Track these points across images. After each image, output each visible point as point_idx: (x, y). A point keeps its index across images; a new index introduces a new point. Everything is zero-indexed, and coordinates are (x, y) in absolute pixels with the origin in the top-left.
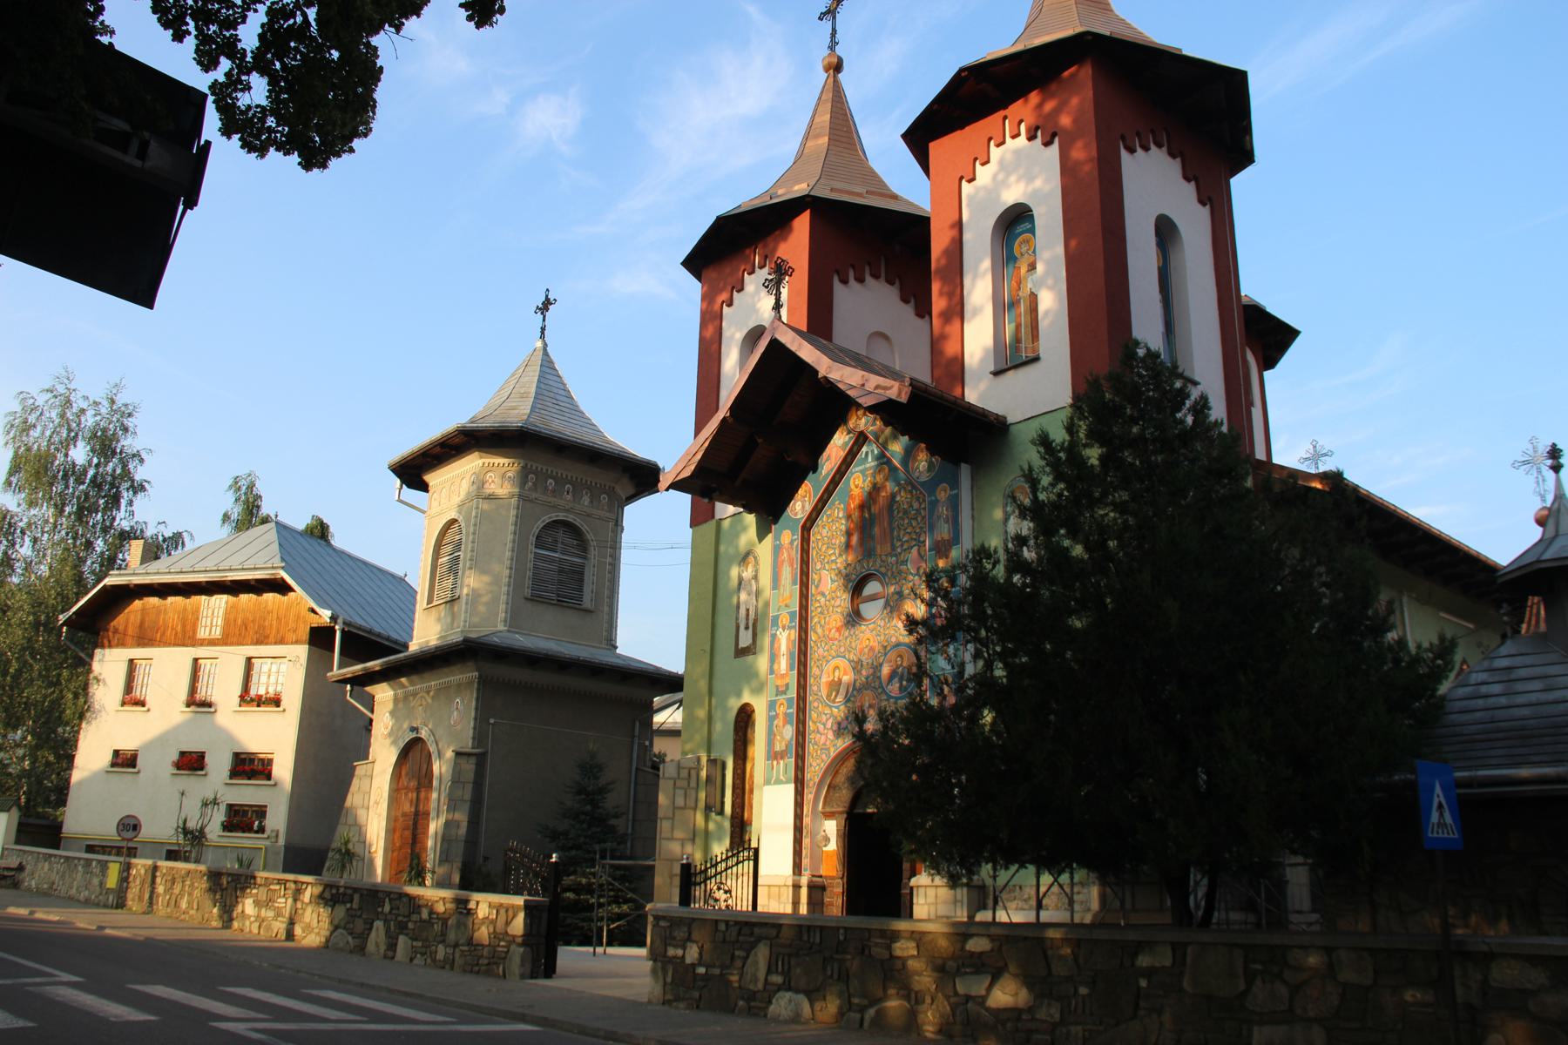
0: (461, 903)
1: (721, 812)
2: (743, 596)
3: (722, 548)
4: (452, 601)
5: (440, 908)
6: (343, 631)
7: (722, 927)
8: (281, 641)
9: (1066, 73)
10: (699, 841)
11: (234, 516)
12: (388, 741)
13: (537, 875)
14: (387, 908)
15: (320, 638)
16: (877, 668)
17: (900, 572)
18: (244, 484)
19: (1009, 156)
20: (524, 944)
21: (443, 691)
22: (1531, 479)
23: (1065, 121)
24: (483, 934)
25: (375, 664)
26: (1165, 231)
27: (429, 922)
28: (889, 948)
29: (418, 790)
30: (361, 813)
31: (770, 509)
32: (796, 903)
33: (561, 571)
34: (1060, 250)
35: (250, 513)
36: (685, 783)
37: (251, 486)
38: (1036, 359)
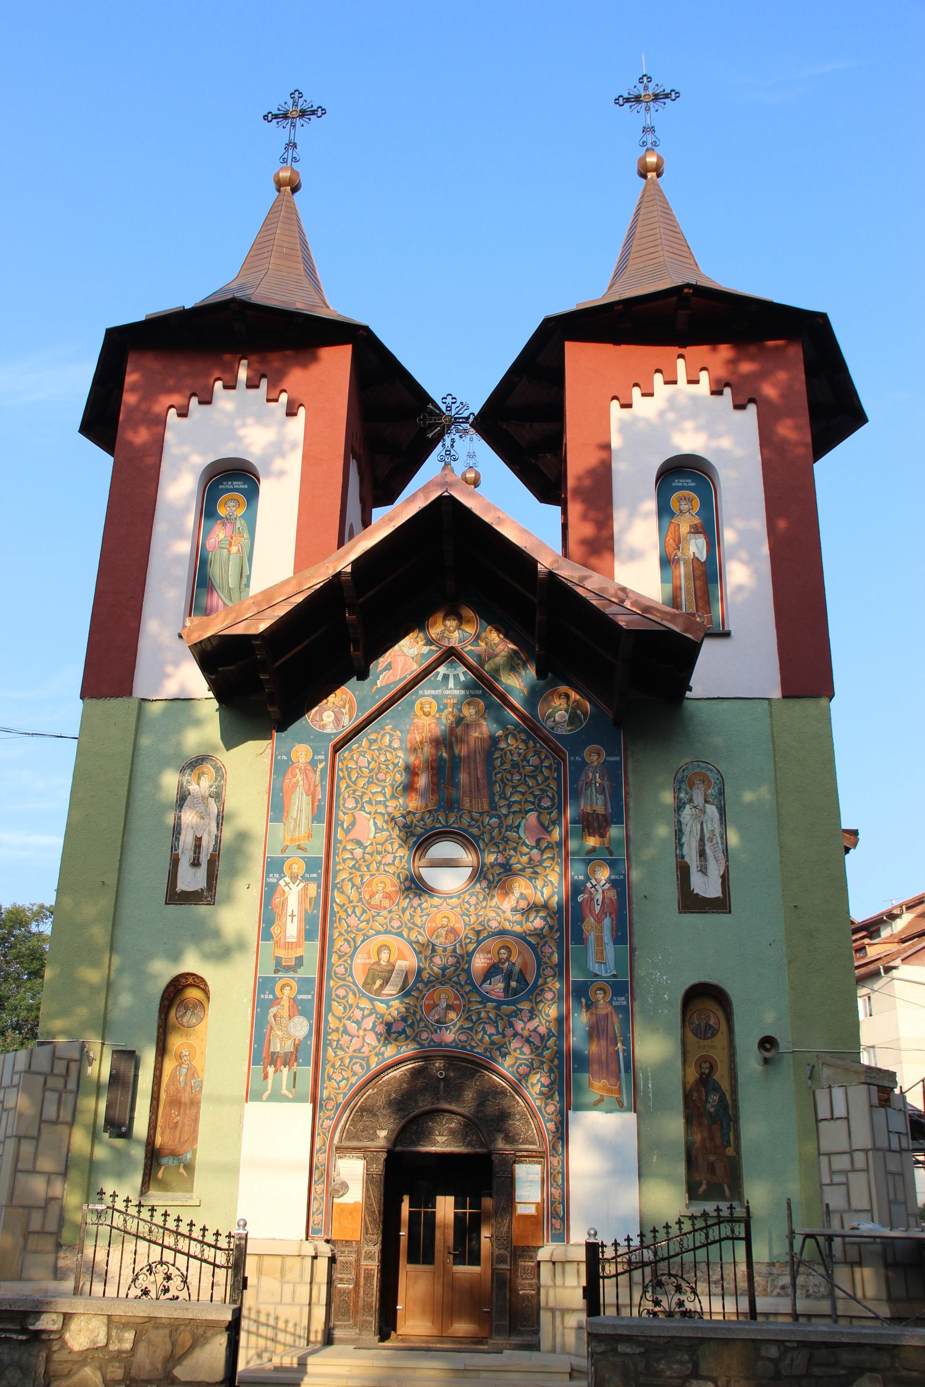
2: (189, 817)
9: (770, 343)
17: (506, 840)
23: (769, 391)
34: (759, 524)
35: (665, 103)
36: (59, 1083)
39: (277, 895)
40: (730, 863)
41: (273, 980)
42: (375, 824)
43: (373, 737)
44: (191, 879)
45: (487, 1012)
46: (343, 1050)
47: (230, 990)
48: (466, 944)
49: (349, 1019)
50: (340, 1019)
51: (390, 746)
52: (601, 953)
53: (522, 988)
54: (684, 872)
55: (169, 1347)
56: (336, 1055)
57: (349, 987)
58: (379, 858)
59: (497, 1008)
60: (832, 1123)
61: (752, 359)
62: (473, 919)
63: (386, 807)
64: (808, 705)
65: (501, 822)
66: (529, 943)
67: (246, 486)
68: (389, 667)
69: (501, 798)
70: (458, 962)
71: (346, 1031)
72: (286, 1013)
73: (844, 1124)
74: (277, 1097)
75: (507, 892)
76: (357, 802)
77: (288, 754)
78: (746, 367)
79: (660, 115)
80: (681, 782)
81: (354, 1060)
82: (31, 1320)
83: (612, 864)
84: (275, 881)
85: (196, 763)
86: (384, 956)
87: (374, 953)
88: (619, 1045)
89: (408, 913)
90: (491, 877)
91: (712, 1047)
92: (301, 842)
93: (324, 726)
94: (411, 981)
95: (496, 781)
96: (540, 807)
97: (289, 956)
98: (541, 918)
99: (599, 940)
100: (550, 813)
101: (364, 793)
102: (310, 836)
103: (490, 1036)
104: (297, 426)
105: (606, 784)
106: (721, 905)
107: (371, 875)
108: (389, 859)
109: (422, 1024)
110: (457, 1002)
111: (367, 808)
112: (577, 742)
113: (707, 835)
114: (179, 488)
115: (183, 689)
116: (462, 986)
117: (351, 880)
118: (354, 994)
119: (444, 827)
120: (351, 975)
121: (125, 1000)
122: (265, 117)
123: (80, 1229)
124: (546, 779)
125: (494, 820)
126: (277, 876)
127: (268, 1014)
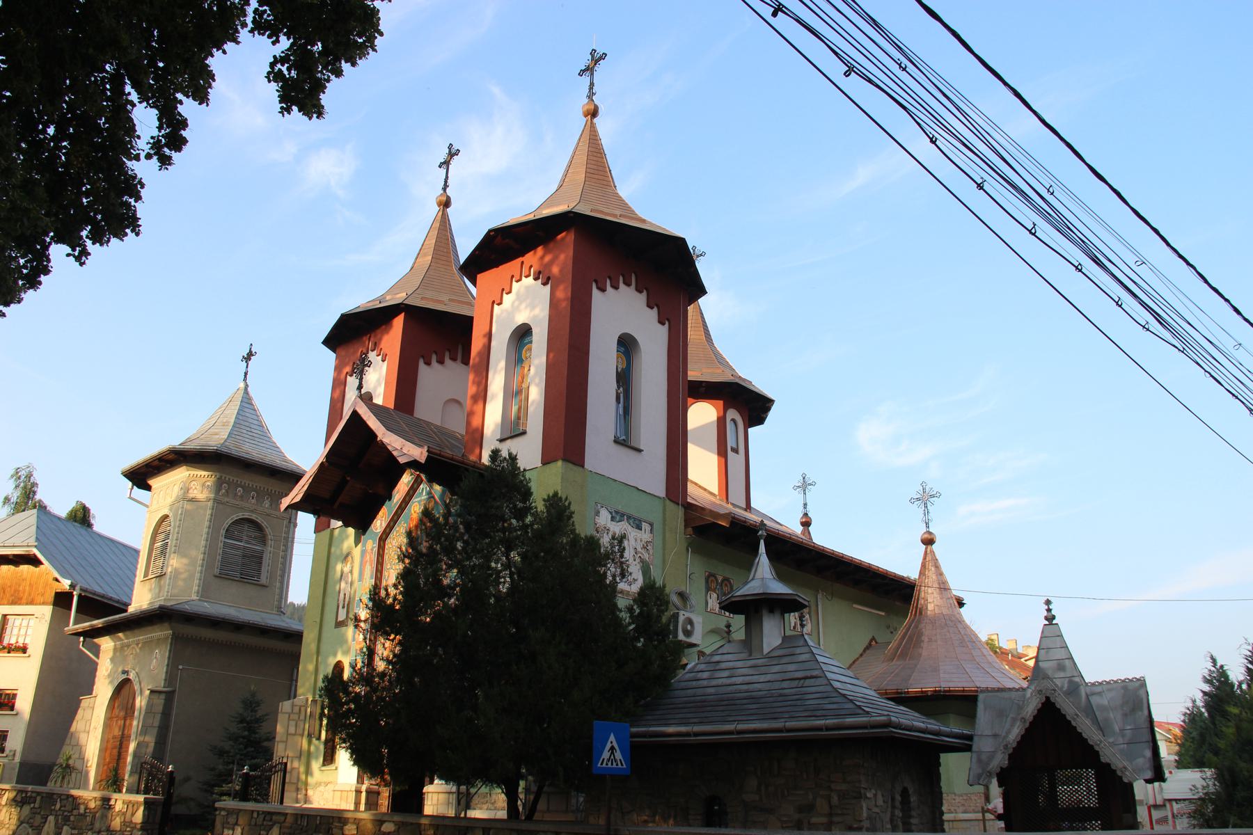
0: (106, 801)
1: (319, 738)
2: (343, 585)
3: (333, 549)
4: (161, 576)
5: (92, 805)
6: (80, 596)
7: (255, 815)
8: (31, 603)
10: (304, 759)
11: (14, 499)
12: (107, 681)
13: (160, 781)
14: (58, 806)
15: (62, 600)
18: (23, 473)
19: (522, 290)
20: (142, 829)
21: (147, 644)
22: (921, 510)
23: (555, 270)
24: (117, 823)
25: (98, 623)
26: (627, 344)
27: (84, 815)
28: (342, 829)
29: (125, 719)
30: (83, 737)
31: (362, 524)
32: (357, 804)
33: (244, 556)
36: (296, 717)
37: (29, 476)
38: (524, 433)
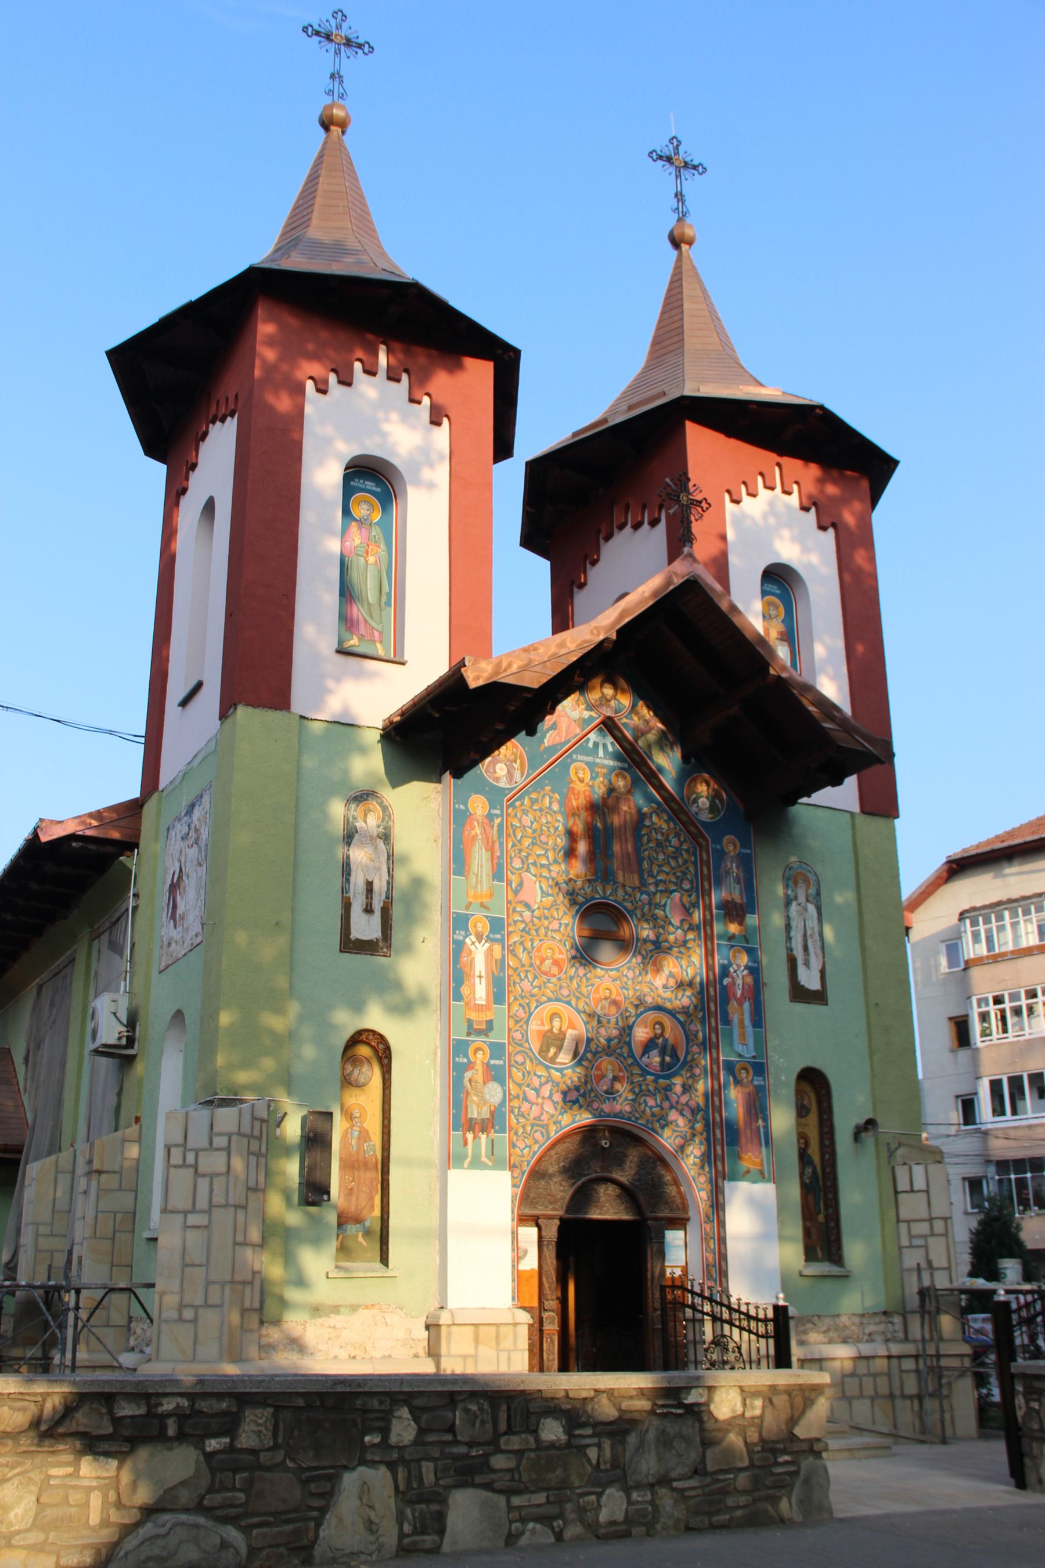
9: (848, 473)
12: (565, 1069)
16: (627, 1030)
17: (655, 918)
39: (464, 954)
40: (826, 959)
41: (467, 1044)
42: (541, 887)
43: (534, 796)
44: (366, 928)
45: (647, 1085)
46: (524, 1117)
47: (418, 1047)
48: (627, 1017)
49: (528, 1086)
50: (519, 1085)
51: (550, 808)
52: (743, 1035)
53: (674, 1060)
54: (792, 962)
55: (789, 1410)
56: (518, 1122)
57: (527, 1054)
58: (546, 923)
59: (655, 1081)
60: (912, 1195)
61: (835, 482)
62: (631, 993)
63: (550, 871)
64: (879, 822)
65: (650, 900)
66: (678, 1020)
67: (379, 490)
68: (554, 727)
69: (649, 876)
70: (620, 1034)
71: (526, 1099)
72: (479, 1077)
73: (924, 1196)
74: (477, 1164)
75: (658, 970)
76: (523, 863)
77: (466, 804)
78: (831, 490)
79: (352, 65)
80: (788, 879)
81: (536, 1128)
82: (683, 1395)
83: (751, 952)
84: (461, 938)
85: (362, 797)
86: (556, 1023)
87: (546, 1021)
88: (760, 1121)
89: (575, 982)
90: (644, 952)
91: (806, 1125)
92: (484, 900)
93: (497, 779)
94: (582, 1051)
95: (644, 859)
96: (682, 888)
97: (479, 1018)
98: (688, 997)
99: (741, 1022)
100: (690, 896)
101: (529, 854)
102: (491, 895)
103: (651, 1108)
104: (442, 436)
105: (741, 874)
106: (819, 997)
107: (541, 940)
108: (555, 925)
109: (593, 1095)
110: (621, 1074)
111: (533, 870)
112: (717, 829)
113: (809, 932)
114: (323, 476)
115: (346, 711)
116: (625, 1059)
117: (522, 943)
118: (531, 1060)
119: (602, 898)
120: (527, 1041)
121: (309, 1052)
122: (305, 29)
123: (284, 1304)
124: (685, 862)
125: (644, 896)
126: (463, 933)
127: (463, 1078)
